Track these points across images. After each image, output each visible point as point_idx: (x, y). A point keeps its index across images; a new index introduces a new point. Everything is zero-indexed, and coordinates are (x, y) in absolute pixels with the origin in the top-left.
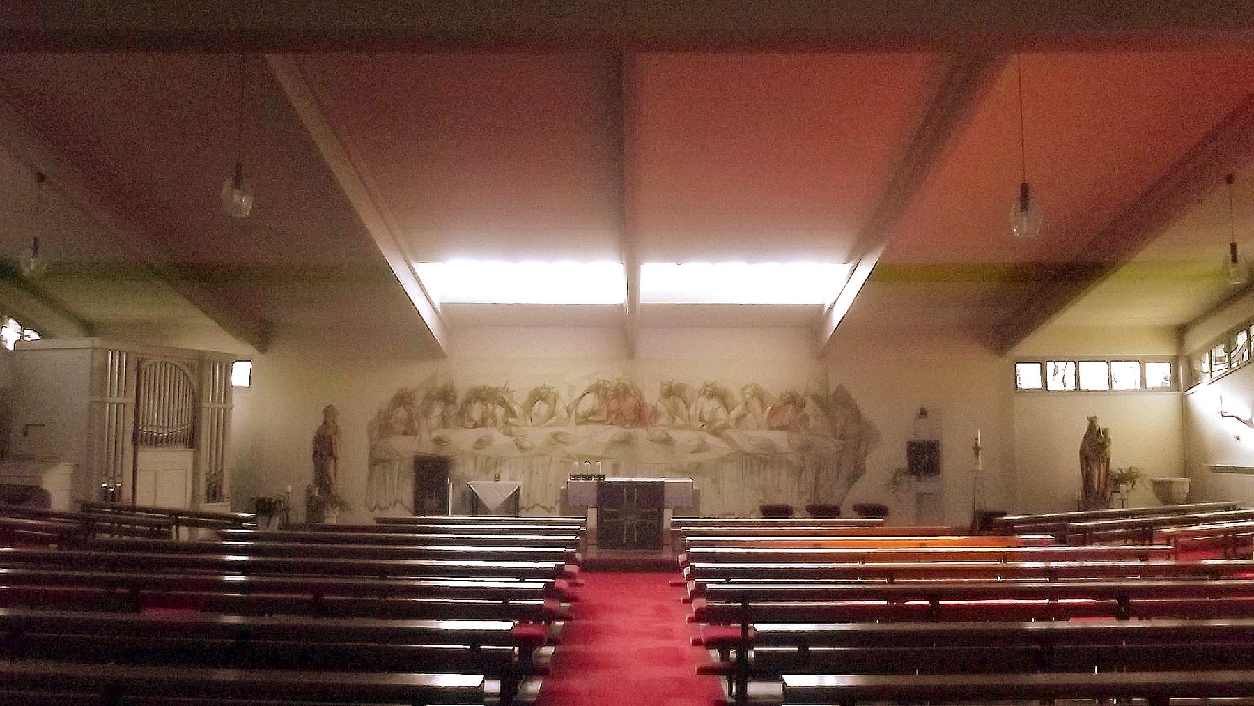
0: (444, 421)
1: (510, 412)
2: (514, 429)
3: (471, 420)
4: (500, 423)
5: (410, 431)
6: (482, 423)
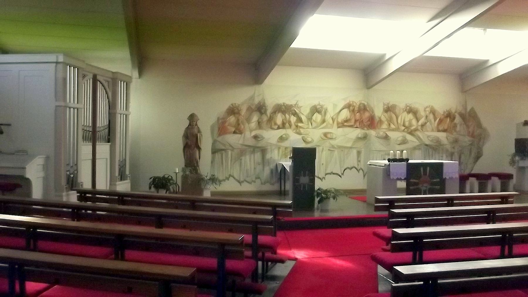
0: (259, 124)
1: (300, 120)
2: (302, 131)
3: (275, 124)
4: (293, 126)
5: (238, 131)
6: (283, 126)
